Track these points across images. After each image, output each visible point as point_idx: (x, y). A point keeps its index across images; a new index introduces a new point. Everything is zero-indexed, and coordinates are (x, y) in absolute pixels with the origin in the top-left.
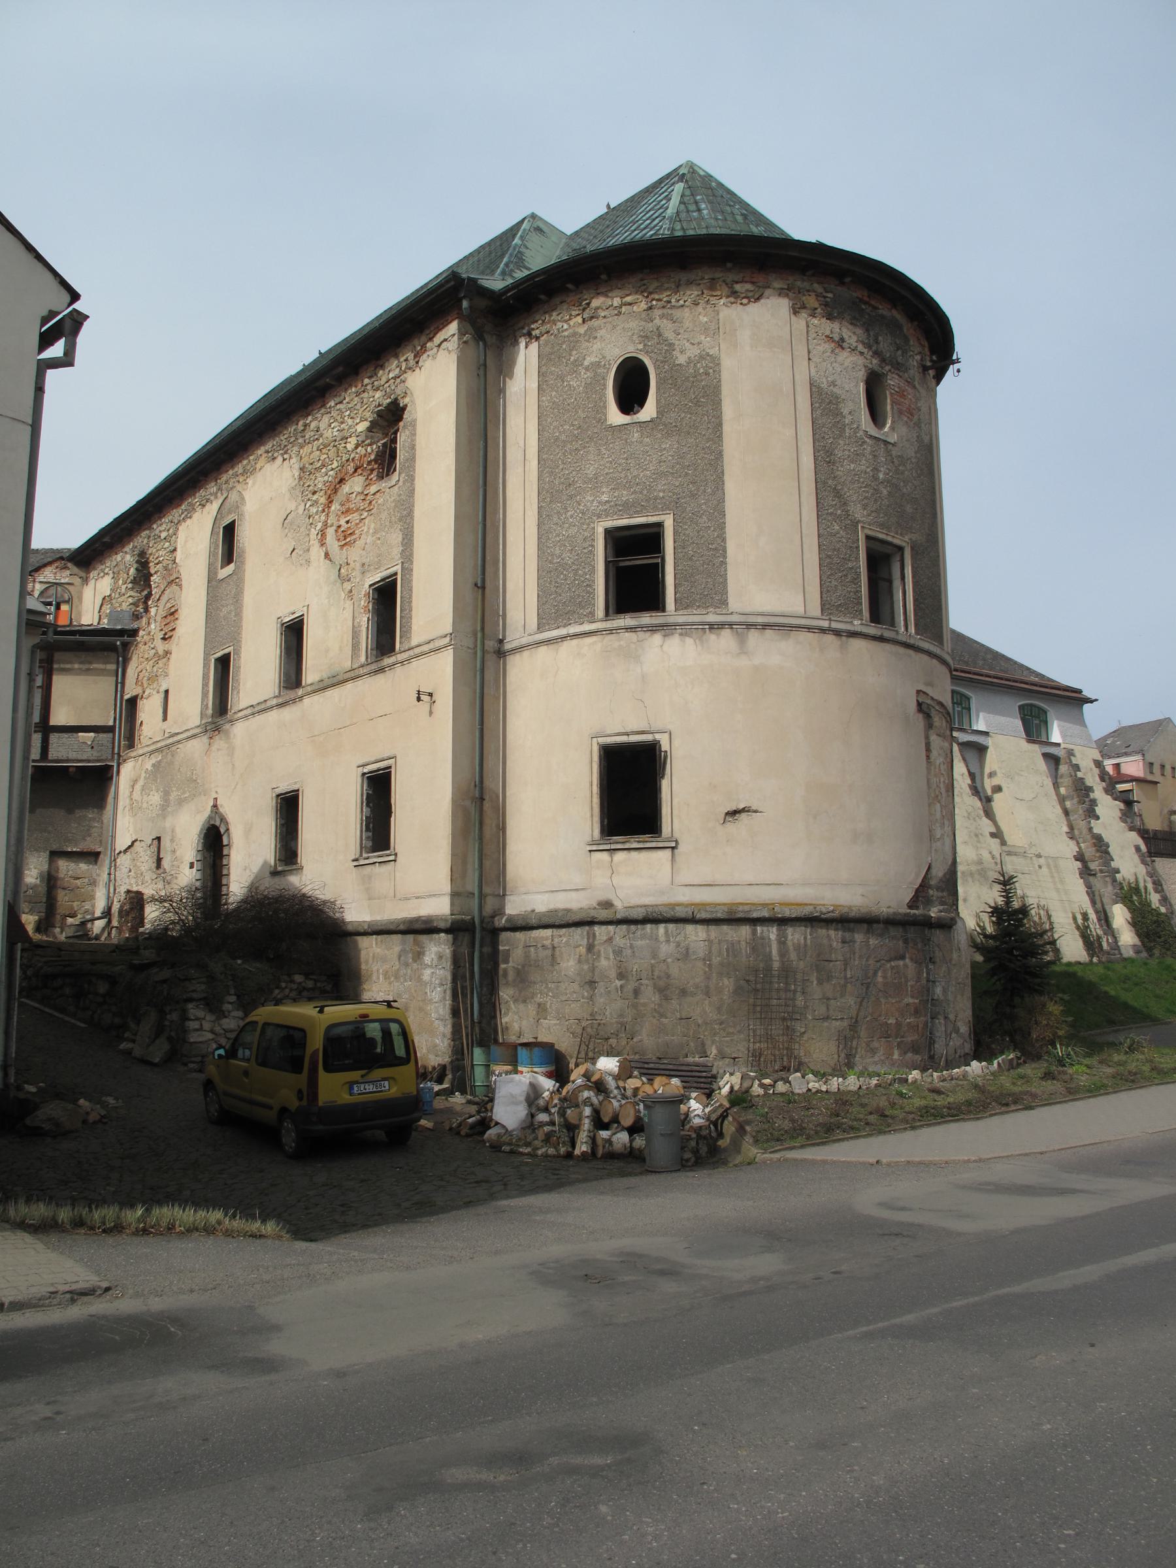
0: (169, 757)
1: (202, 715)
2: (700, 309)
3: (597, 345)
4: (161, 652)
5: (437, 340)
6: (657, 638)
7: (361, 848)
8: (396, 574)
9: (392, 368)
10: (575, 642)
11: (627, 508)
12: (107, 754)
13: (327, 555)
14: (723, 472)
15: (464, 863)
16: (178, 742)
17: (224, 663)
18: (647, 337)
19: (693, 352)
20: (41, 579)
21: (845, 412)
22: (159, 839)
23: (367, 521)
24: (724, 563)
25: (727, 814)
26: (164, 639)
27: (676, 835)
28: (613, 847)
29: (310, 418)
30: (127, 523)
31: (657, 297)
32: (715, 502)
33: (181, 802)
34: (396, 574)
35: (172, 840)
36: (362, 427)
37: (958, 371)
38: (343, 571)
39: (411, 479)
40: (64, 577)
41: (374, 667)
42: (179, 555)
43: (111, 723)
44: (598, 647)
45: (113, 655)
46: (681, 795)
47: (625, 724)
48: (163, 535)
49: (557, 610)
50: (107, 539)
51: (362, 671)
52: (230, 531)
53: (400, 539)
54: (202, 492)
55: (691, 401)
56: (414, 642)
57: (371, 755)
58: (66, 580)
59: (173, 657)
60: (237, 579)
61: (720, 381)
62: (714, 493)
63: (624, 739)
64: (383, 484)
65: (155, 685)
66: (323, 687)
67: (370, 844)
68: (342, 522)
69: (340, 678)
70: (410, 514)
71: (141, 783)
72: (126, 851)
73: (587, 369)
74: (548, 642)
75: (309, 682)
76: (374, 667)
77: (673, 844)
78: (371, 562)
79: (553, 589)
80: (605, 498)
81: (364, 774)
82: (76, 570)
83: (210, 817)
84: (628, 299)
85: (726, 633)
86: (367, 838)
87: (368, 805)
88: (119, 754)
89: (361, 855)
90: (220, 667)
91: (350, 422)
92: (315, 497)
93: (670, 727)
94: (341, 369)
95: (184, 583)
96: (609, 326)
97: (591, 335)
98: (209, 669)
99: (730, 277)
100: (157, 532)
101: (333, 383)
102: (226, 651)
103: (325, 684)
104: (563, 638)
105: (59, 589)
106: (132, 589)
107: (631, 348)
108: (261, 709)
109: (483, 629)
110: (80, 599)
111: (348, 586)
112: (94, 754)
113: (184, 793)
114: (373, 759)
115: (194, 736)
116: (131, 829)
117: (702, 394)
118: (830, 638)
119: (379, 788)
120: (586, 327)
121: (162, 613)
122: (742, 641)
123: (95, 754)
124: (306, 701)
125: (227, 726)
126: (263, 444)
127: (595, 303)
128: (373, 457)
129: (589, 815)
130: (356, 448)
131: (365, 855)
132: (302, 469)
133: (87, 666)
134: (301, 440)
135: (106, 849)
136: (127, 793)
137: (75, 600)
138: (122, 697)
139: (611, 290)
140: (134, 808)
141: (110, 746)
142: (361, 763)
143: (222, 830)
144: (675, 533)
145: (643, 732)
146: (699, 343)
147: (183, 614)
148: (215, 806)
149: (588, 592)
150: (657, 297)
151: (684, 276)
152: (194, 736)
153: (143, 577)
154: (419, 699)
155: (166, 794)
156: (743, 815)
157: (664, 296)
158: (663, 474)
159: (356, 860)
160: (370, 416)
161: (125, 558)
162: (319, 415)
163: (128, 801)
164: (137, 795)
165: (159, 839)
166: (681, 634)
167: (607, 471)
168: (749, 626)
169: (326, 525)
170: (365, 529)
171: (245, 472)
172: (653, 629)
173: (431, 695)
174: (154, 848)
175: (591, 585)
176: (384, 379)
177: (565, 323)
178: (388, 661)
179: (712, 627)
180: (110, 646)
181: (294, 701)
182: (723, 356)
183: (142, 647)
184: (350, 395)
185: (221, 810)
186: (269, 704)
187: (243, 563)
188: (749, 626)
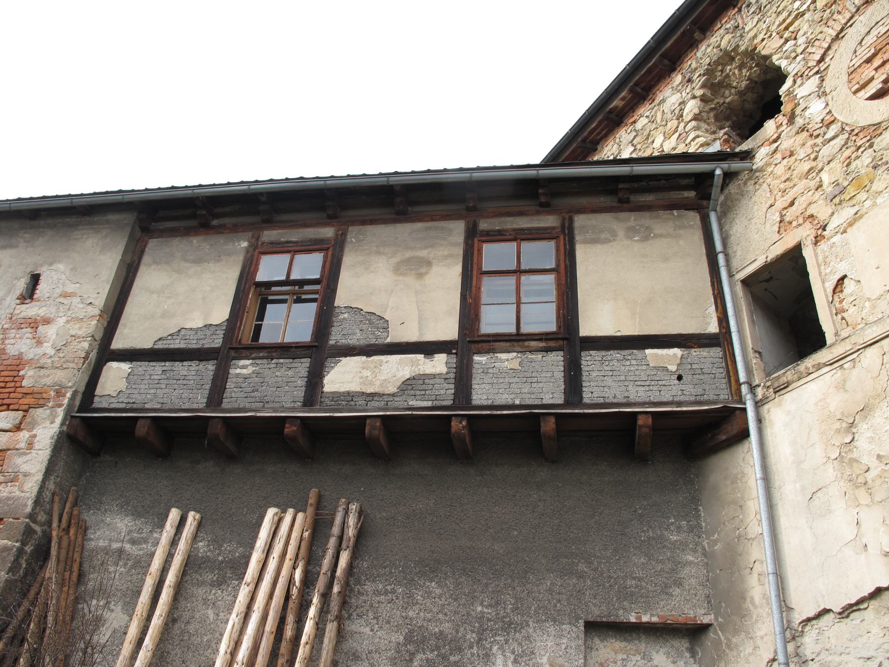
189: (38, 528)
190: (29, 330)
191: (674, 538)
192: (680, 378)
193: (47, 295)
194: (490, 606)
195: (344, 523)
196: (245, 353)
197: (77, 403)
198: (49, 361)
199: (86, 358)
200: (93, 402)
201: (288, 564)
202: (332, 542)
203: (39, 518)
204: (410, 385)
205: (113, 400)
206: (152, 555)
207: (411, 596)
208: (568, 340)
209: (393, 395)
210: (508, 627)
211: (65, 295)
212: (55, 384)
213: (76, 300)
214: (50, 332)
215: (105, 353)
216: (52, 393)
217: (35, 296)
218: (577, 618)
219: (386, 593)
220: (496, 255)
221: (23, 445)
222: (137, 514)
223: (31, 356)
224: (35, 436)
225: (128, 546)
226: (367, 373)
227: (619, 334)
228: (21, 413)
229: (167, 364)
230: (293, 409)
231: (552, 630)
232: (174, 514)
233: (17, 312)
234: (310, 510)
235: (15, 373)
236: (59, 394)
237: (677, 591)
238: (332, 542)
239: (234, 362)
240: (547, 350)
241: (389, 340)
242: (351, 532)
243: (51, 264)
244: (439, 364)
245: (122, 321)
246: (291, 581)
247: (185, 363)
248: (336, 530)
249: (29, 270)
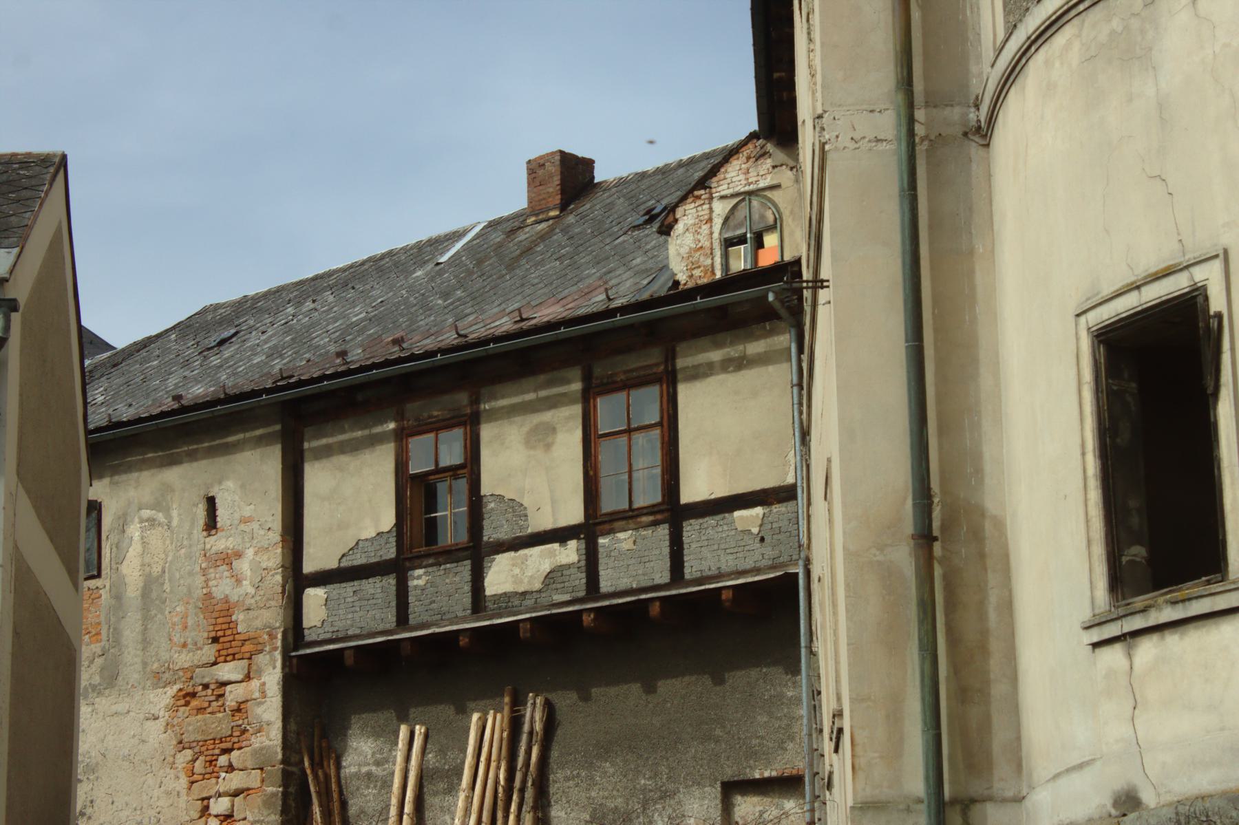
123: (769, 552)
189: (294, 769)
190: (225, 567)
191: (790, 694)
192: (762, 539)
193: (228, 522)
194: (650, 778)
195: (532, 717)
196: (417, 562)
197: (291, 639)
198: (253, 601)
199: (283, 592)
200: (304, 636)
201: (493, 765)
202: (524, 738)
203: (293, 760)
204: (554, 576)
205: (320, 631)
206: (393, 773)
207: (592, 778)
208: (674, 512)
209: (540, 591)
210: (665, 795)
211: (245, 520)
212: (265, 627)
213: (255, 526)
214: (244, 566)
215: (298, 580)
216: (266, 637)
217: (219, 525)
218: (716, 780)
219: (573, 778)
220: (609, 410)
221: (257, 695)
222: (376, 735)
223: (236, 598)
224: (264, 684)
225: (374, 768)
226: (517, 571)
227: (713, 497)
228: (245, 662)
229: (356, 583)
230: (457, 620)
231: (697, 793)
232: (404, 730)
233: (208, 546)
234: (507, 709)
235: (228, 619)
236: (272, 636)
237: (790, 746)
238: (524, 738)
239: (410, 573)
240: (655, 524)
241: (530, 531)
242: (538, 727)
243: (220, 483)
244: (570, 553)
245: (306, 539)
246: (497, 782)
247: (371, 580)
248: (526, 728)
249: (202, 493)
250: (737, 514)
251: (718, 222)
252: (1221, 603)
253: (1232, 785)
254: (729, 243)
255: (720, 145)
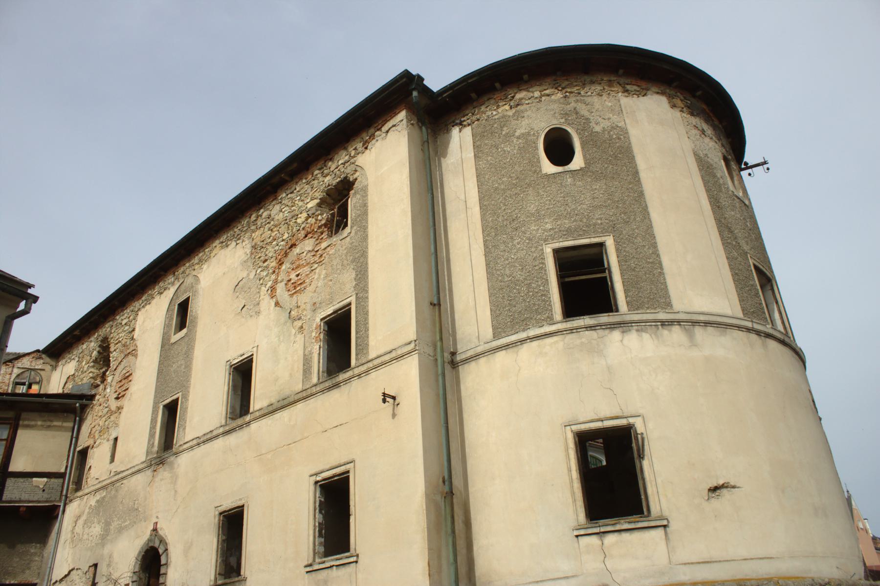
0: (113, 492)
1: (148, 453)
2: (605, 97)
3: (525, 122)
4: (113, 408)
5: (385, 128)
6: (616, 335)
7: (315, 553)
8: (350, 304)
9: (342, 157)
10: (535, 344)
11: (569, 233)
12: (55, 496)
13: (277, 304)
14: (646, 205)
15: (439, 557)
16: (122, 478)
17: (172, 410)
18: (566, 114)
19: (606, 124)
20: (20, 365)
21: (719, 176)
22: (96, 565)
23: (317, 271)
24: (662, 274)
25: (710, 490)
26: (117, 398)
27: (666, 513)
28: (603, 529)
29: (262, 211)
30: (96, 317)
31: (569, 90)
32: (645, 228)
33: (120, 530)
34: (350, 304)
35: (109, 565)
36: (312, 204)
37: (768, 169)
38: (293, 313)
39: (364, 229)
40: (38, 364)
41: (328, 384)
42: (136, 334)
43: (63, 470)
44: (561, 345)
45: (72, 416)
46: (663, 474)
47: (599, 410)
48: (124, 322)
49: (512, 318)
50: (77, 333)
51: (314, 390)
52: (184, 308)
53: (354, 275)
54: (161, 284)
55: (610, 156)
56: (372, 354)
57: (327, 464)
58: (40, 367)
59: (124, 411)
60: (190, 342)
61: (630, 143)
62: (642, 221)
63: (598, 425)
64: (335, 239)
65: (105, 436)
66: (271, 411)
67: (322, 549)
68: (293, 276)
69: (291, 399)
70: (364, 254)
71: (84, 518)
72: (61, 580)
73: (518, 138)
74: (506, 347)
75: (257, 407)
76: (328, 384)
77: (665, 523)
78: (322, 297)
79: (507, 303)
80: (549, 226)
81: (316, 482)
82: (48, 360)
83: (149, 540)
84: (547, 92)
85: (676, 329)
86: (320, 544)
87: (320, 512)
88: (66, 497)
89: (314, 561)
90: (167, 413)
91: (300, 204)
92: (266, 264)
93: (641, 411)
94: (295, 165)
95: (139, 353)
96: (534, 109)
97: (519, 116)
98: (156, 422)
99: (622, 80)
100: (119, 321)
101: (287, 178)
102: (175, 397)
103: (274, 407)
104: (522, 341)
105: (33, 373)
106: (93, 367)
107: (555, 122)
108: (209, 438)
109: (441, 339)
110: (49, 381)
111: (298, 324)
112: (45, 496)
113: (125, 522)
114: (328, 467)
115: (139, 471)
116: (70, 560)
117: (617, 154)
118: (754, 337)
119: (335, 496)
120: (514, 110)
121: (117, 378)
122: (691, 337)
124: (254, 426)
125: (172, 458)
126: (219, 238)
127: (518, 96)
128: (323, 222)
129: (570, 500)
130: (307, 219)
131: (318, 560)
132: (254, 247)
133: (49, 423)
134: (253, 228)
135: (43, 580)
136: (70, 528)
137: (44, 382)
138: (75, 449)
139: (532, 87)
140: (75, 540)
141: (59, 489)
142: (313, 472)
143: (161, 551)
144: (617, 250)
145: (617, 418)
146: (609, 119)
147: (136, 377)
148: (155, 530)
149: (544, 300)
150: (569, 90)
151: (588, 78)
152: (139, 471)
153: (104, 359)
154: (384, 401)
155: (108, 524)
156: (724, 491)
157: (575, 89)
158: (596, 207)
159: (310, 565)
160: (319, 195)
161: (91, 346)
162: (271, 207)
163: (69, 535)
164: (79, 529)
165: (96, 565)
166: (637, 331)
167: (547, 207)
168: (695, 323)
169: (276, 282)
170: (316, 276)
171: (200, 261)
172: (612, 326)
173: (394, 398)
174: (90, 575)
175: (546, 294)
176: (333, 167)
177: (496, 111)
178: (342, 376)
179: (664, 323)
180: (72, 407)
181: (241, 427)
182: (629, 127)
183: (97, 408)
184: (301, 186)
185: (161, 532)
186: (215, 433)
187: (195, 326)
188: (695, 323)
237: (27, 572)
250: (34, 479)
251: (14, 376)
252: (645, 524)
253: (478, 584)
254: (17, 384)
255: (18, 352)
